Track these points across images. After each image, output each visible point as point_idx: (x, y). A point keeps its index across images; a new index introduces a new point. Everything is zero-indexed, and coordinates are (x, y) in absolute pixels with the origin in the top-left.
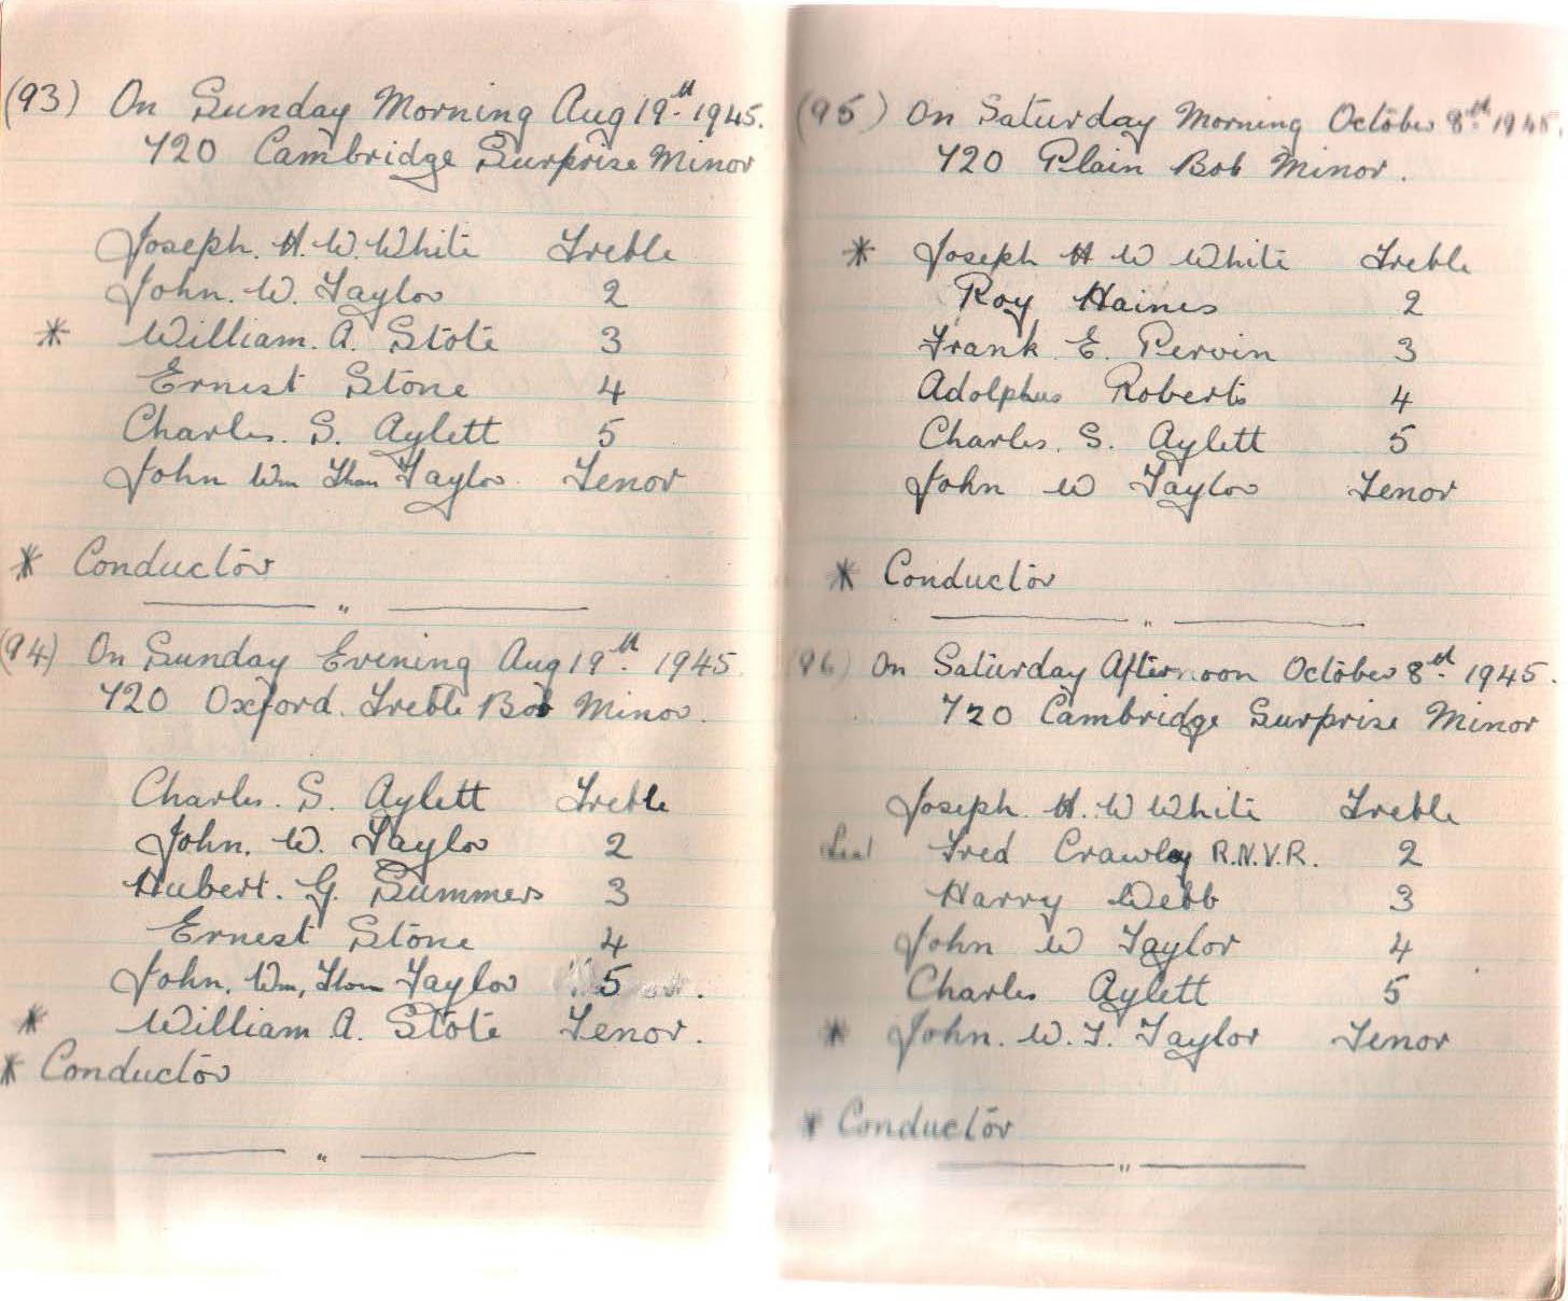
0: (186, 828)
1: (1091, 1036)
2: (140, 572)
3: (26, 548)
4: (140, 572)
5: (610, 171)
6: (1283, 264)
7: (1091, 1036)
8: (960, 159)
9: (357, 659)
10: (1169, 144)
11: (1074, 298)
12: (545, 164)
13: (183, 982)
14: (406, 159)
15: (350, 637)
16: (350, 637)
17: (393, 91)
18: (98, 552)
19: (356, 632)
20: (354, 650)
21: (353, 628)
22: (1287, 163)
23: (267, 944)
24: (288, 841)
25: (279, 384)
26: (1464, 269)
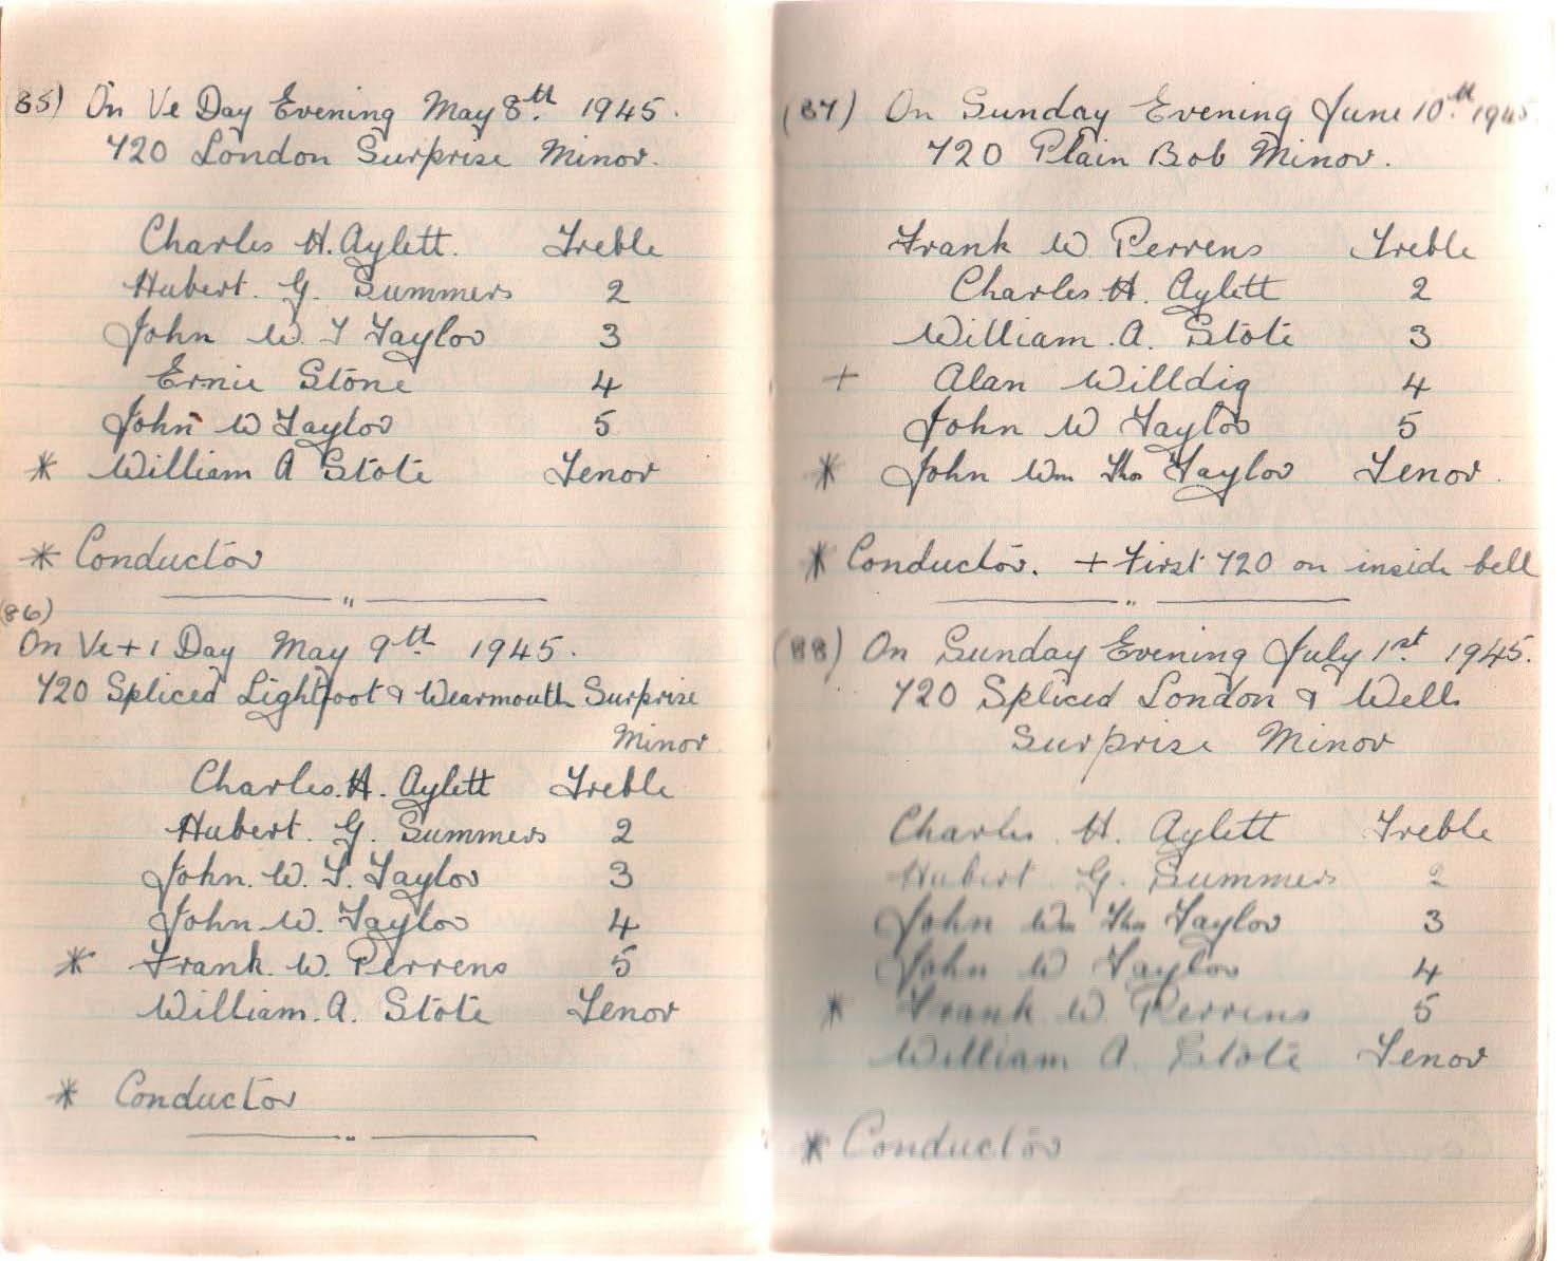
0: (929, 908)
2: (1024, 657)
4: (1024, 657)
6: (1069, 248)
8: (950, 154)
10: (410, 133)
11: (124, 284)
18: (959, 640)
22: (1270, 152)
23: (241, 974)
24: (275, 876)
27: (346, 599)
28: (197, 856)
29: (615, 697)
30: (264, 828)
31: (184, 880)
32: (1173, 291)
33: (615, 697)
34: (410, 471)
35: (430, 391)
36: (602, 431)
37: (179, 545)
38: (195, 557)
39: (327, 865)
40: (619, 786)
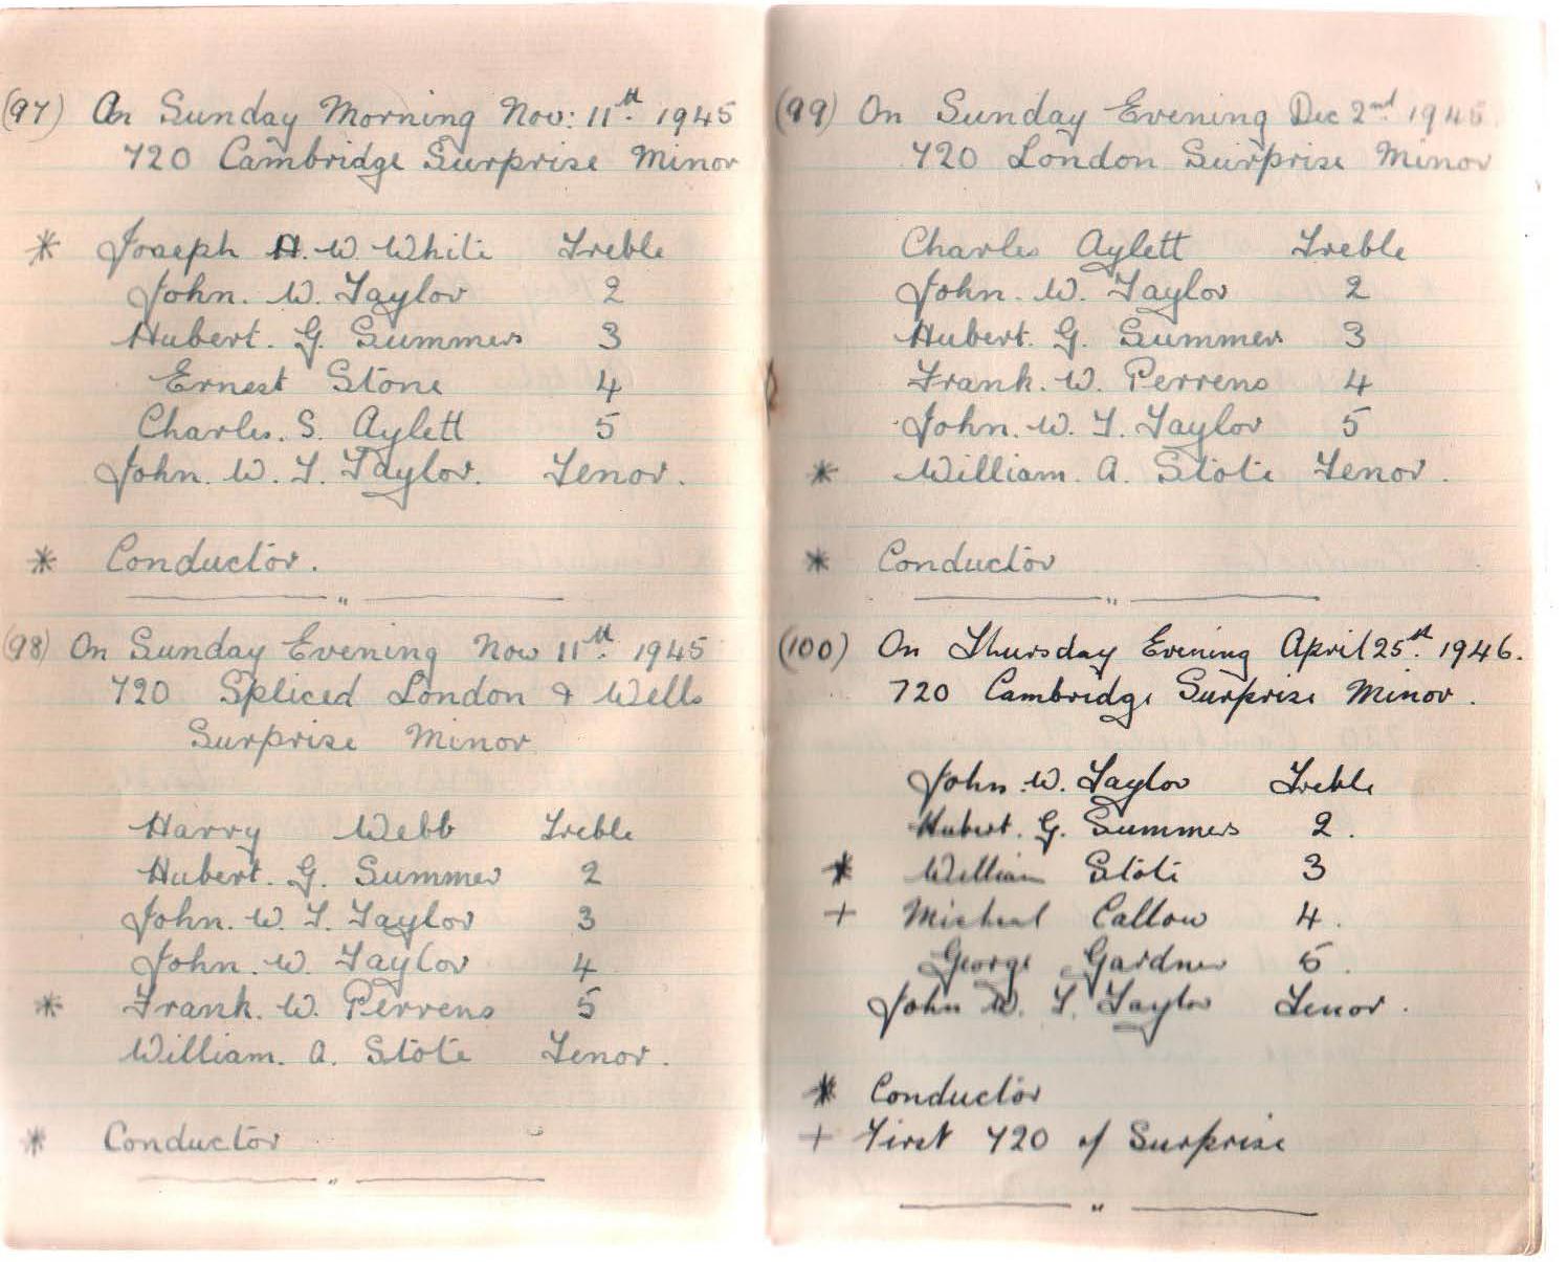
1: (1101, 427)
3: (42, 549)
5: (568, 173)
7: (1101, 427)
9: (322, 649)
12: (489, 164)
13: (193, 965)
14: (358, 163)
15: (313, 627)
16: (313, 627)
17: (339, 102)
19: (318, 623)
20: (318, 639)
21: (315, 619)
25: (271, 385)
26: (1398, 255)
27: (1115, 604)
28: (170, 900)
29: (224, 741)
30: (984, 828)
31: (162, 924)
32: (99, 113)
33: (224, 741)
34: (1253, 471)
35: (555, 349)
36: (1350, 431)
37: (982, 547)
38: (998, 561)
39: (354, 907)
40: (591, 830)
